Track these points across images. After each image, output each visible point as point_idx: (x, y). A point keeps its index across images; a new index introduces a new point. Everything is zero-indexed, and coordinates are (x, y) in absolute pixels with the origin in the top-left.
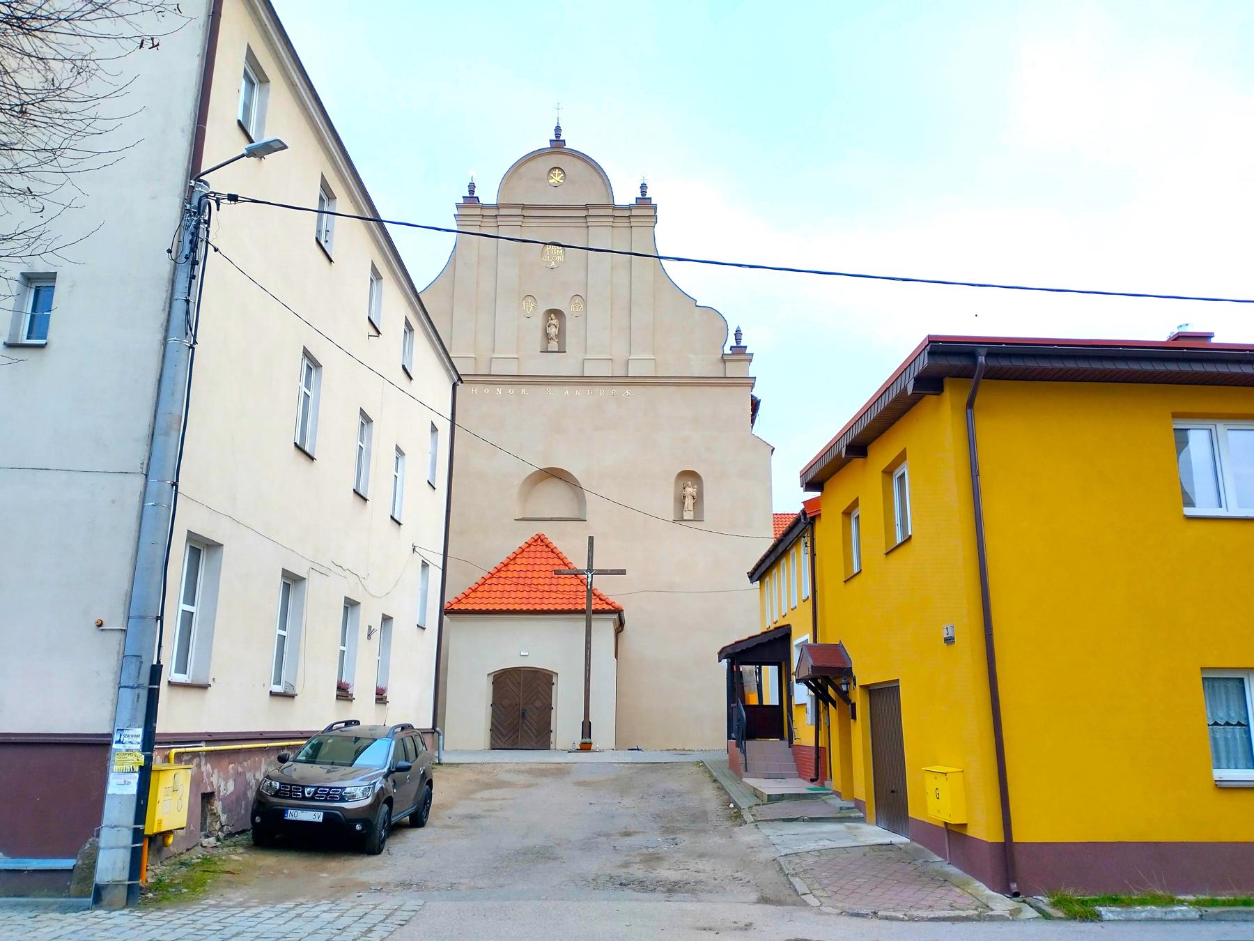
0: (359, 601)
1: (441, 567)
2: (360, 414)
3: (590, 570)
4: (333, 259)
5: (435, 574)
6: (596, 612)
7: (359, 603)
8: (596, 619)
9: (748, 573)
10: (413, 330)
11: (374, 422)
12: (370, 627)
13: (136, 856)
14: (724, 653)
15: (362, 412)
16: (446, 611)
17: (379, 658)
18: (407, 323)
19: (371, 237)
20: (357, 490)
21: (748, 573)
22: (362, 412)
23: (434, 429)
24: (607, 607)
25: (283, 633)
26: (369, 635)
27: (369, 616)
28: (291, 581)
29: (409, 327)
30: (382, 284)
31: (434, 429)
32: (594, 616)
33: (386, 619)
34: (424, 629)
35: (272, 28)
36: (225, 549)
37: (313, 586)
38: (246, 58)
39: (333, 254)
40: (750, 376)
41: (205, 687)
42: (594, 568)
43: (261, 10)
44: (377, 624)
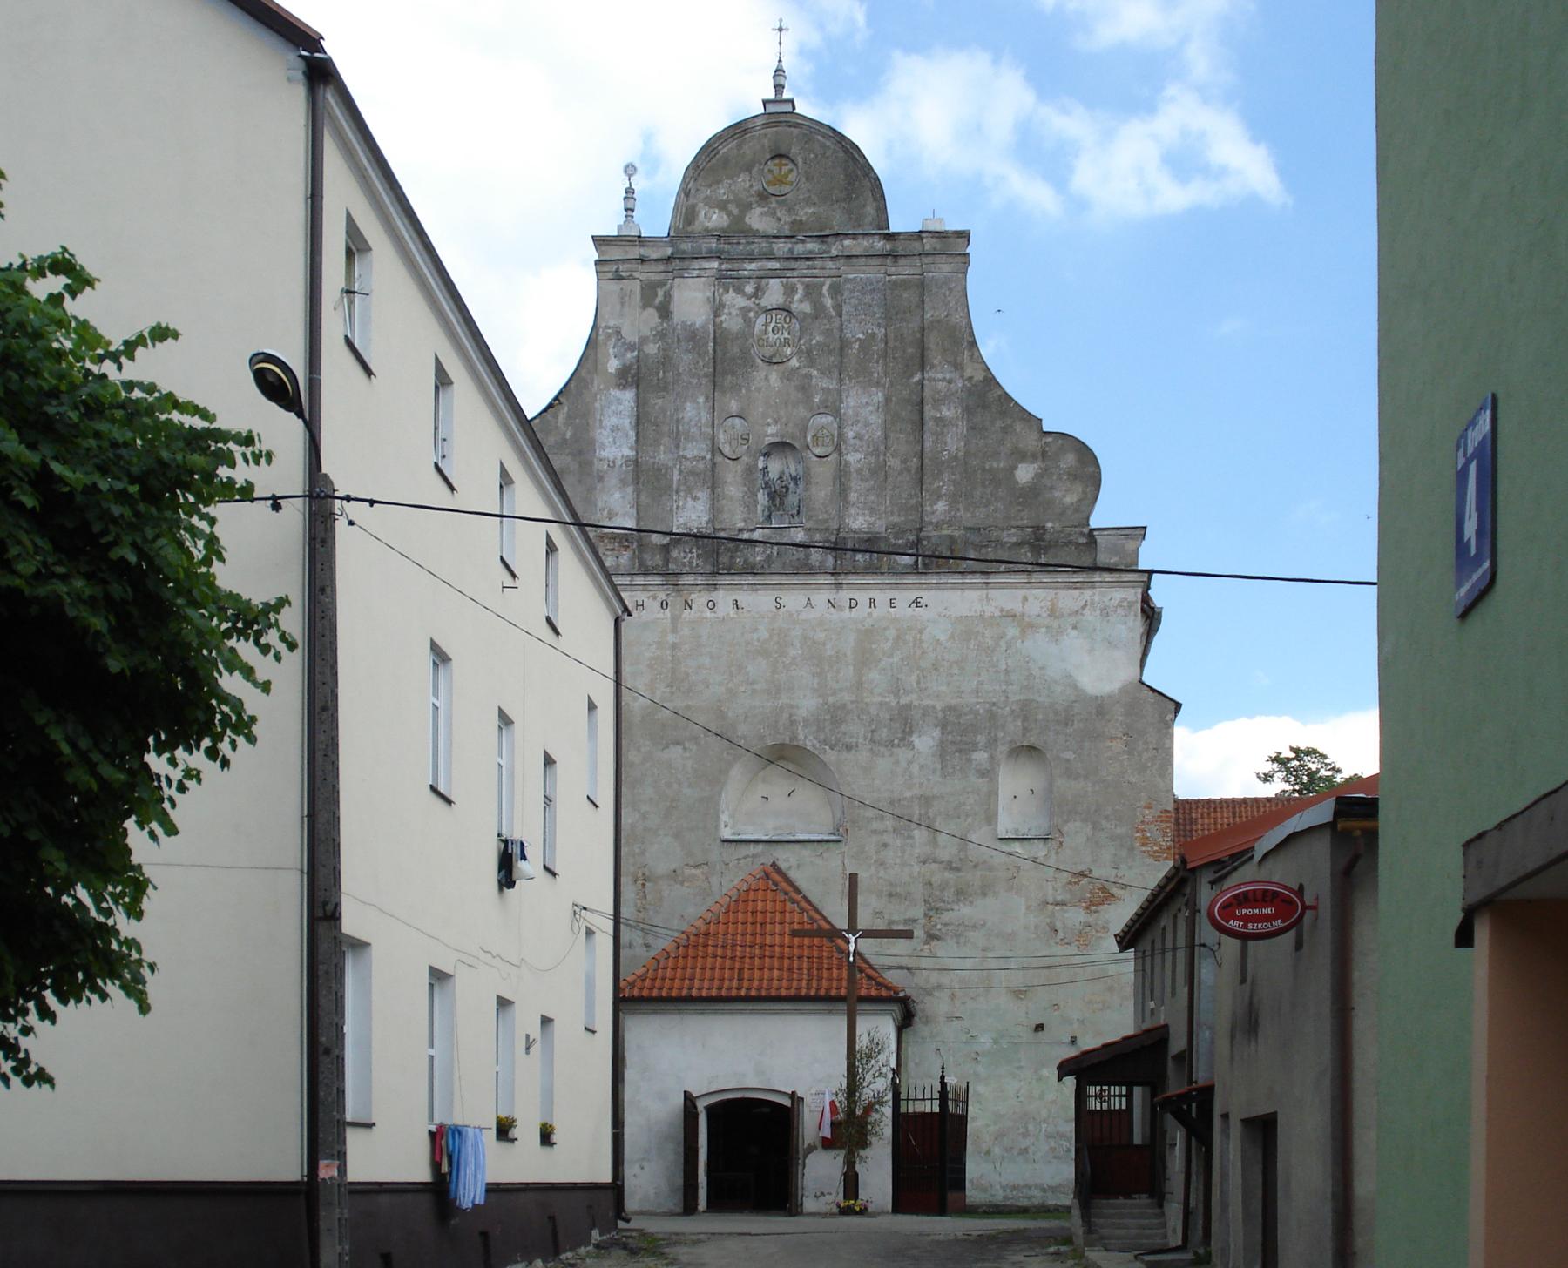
0: (367, 940)
1: (612, 933)
2: (432, 648)
3: (852, 928)
4: (374, 370)
5: (605, 944)
6: (862, 1000)
7: (369, 944)
8: (865, 1012)
9: (1115, 936)
10: (557, 550)
11: (558, 764)
12: (528, 1036)
13: (1027, 1131)
14: (1065, 1069)
15: (434, 647)
16: (626, 1001)
17: (498, 1069)
18: (504, 473)
19: (395, 247)
20: (435, 786)
21: (1115, 936)
22: (434, 647)
23: (592, 707)
24: (884, 993)
25: (432, 1052)
26: (528, 1049)
27: (526, 1021)
28: (438, 977)
29: (442, 380)
30: (514, 491)
31: (592, 707)
32: (860, 1007)
33: (546, 1021)
34: (594, 1032)
35: (467, 338)
36: (516, 1005)
37: (463, 981)
38: (347, 232)
39: (560, 622)
40: (1140, 568)
41: (370, 1126)
42: (859, 928)
43: (395, 216)
44: (535, 1031)
